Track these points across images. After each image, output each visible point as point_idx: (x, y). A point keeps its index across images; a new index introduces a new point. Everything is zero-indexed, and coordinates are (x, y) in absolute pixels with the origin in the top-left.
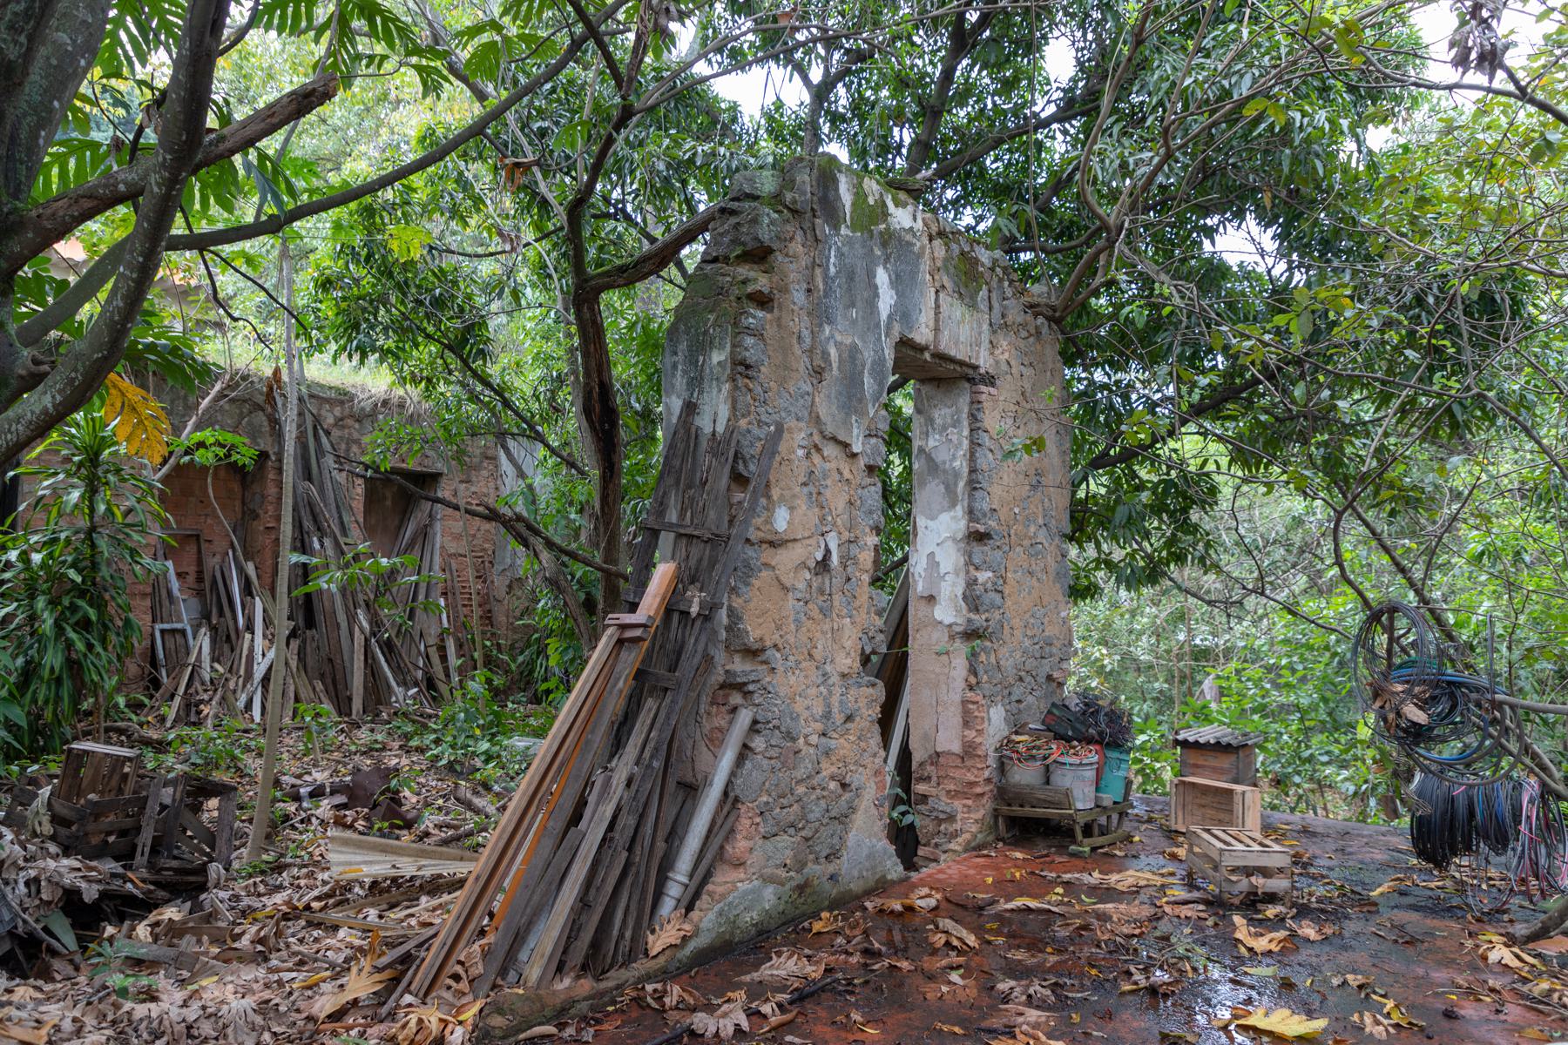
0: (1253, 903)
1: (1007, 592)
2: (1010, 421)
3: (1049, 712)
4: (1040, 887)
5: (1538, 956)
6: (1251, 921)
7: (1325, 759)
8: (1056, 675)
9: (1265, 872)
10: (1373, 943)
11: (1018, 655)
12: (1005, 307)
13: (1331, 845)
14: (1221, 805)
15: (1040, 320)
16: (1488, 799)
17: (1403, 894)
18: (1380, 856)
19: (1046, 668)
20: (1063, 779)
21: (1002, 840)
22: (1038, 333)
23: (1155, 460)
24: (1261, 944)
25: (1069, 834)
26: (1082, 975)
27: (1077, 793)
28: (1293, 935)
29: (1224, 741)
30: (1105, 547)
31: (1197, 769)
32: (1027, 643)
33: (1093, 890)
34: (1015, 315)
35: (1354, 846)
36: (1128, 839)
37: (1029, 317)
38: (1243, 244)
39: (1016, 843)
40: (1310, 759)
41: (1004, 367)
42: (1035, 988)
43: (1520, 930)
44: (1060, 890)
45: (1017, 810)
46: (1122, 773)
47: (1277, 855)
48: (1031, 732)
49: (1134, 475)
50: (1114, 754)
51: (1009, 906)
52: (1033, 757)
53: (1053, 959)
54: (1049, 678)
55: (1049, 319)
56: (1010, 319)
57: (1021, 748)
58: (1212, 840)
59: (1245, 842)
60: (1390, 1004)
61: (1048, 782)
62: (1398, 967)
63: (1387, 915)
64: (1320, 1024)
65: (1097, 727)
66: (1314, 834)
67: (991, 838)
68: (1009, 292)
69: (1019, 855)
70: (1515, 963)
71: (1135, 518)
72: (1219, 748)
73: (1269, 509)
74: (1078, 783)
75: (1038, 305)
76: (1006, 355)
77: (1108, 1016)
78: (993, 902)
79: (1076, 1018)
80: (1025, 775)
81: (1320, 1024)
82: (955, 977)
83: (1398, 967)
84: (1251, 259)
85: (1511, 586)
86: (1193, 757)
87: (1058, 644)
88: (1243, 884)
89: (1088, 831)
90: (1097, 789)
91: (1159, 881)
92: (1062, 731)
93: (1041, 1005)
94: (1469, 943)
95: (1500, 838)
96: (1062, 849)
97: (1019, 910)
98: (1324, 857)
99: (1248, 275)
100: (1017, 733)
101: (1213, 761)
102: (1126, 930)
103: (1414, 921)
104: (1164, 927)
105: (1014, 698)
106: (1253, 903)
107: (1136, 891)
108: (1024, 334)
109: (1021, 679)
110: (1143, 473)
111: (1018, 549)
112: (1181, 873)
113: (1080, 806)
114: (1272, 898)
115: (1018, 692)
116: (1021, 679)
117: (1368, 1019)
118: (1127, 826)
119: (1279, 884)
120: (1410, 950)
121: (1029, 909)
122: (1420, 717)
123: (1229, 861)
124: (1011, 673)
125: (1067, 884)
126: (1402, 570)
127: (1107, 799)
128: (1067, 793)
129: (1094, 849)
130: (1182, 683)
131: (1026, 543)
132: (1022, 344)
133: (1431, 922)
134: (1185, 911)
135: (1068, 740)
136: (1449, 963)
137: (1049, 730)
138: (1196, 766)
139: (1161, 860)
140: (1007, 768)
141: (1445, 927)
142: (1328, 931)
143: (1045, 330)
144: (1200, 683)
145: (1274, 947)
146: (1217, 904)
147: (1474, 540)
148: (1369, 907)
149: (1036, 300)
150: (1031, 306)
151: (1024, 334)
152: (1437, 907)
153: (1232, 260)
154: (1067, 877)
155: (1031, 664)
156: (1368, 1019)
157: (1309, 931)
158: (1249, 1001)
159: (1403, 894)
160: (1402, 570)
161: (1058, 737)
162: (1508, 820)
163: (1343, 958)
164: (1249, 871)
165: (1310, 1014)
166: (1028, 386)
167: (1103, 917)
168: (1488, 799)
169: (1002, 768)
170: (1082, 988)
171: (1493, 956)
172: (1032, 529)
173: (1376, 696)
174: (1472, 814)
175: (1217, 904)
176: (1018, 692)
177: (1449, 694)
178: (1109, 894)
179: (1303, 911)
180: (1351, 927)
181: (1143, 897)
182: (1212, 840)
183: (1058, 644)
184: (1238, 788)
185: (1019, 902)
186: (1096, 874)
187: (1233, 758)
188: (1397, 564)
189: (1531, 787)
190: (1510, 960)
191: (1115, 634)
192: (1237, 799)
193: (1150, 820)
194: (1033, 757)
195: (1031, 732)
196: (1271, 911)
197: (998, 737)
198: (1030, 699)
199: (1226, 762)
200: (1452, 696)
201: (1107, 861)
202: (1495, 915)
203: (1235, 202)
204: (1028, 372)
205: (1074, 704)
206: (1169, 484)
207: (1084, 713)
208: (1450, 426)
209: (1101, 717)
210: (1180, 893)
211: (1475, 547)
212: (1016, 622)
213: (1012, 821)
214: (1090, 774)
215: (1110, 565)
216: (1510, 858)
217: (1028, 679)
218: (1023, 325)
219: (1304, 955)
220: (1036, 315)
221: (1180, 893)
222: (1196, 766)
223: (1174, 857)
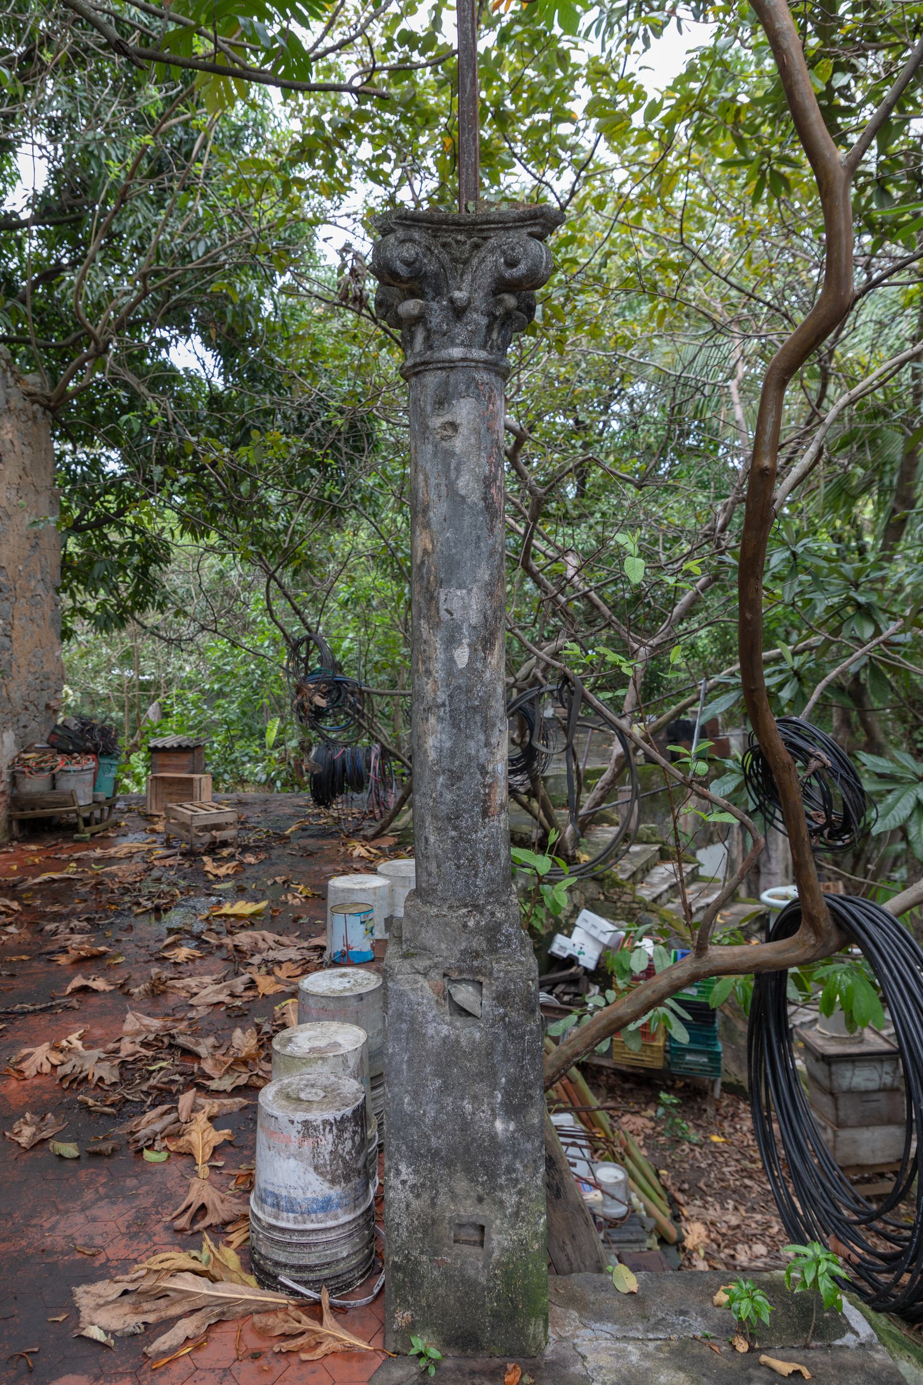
0: (213, 848)
1: (14, 636)
2: (14, 492)
3: (53, 733)
4: (61, 865)
5: (379, 848)
6: (214, 860)
7: (245, 759)
8: (52, 703)
9: (218, 827)
10: (288, 860)
11: (24, 688)
12: (8, 395)
13: (258, 809)
14: (185, 789)
15: (36, 406)
16: (353, 759)
17: (304, 830)
18: (289, 811)
19: (44, 700)
20: (66, 784)
21: (16, 839)
22: (35, 417)
23: (120, 527)
24: (222, 871)
25: (74, 828)
26: (105, 910)
27: (79, 793)
28: (241, 863)
29: (184, 744)
30: (78, 597)
31: (164, 767)
32: (31, 678)
33: (98, 861)
34: (17, 402)
35: (272, 807)
36: (117, 825)
37: (27, 404)
38: (189, 355)
39: (28, 840)
40: (234, 761)
41: (9, 446)
42: (75, 923)
43: (370, 832)
44: (73, 864)
45: (29, 814)
46: (112, 775)
47: (229, 815)
48: (37, 750)
49: (105, 536)
50: (106, 761)
51: (37, 880)
52: (42, 769)
53: (81, 906)
54: (48, 707)
55: (46, 408)
56: (12, 404)
57: (31, 763)
58: (185, 811)
59: (206, 807)
60: (301, 887)
61: (54, 788)
62: (304, 868)
63: (295, 844)
64: (263, 904)
65: (91, 740)
66: (246, 804)
67: (6, 839)
68: (11, 381)
69: (33, 847)
70: (366, 854)
71: (112, 573)
72: (181, 750)
73: (196, 563)
74: (80, 783)
75: (35, 394)
76: (10, 436)
77: (130, 928)
78: (23, 881)
79: (109, 934)
80: (35, 785)
81: (263, 904)
82: (11, 929)
83: (304, 868)
84: (194, 365)
85: (367, 624)
86: (160, 759)
87: (53, 678)
88: (207, 837)
89: (87, 822)
90: (94, 789)
91: (146, 847)
92: (64, 747)
93: (82, 931)
94: (342, 849)
95: (359, 783)
96: (67, 839)
97: (46, 882)
98: (254, 815)
99: (192, 379)
100: (25, 752)
101: (175, 760)
102: (130, 880)
103: (311, 843)
104: (156, 873)
105: (21, 724)
106: (213, 848)
107: (130, 857)
108: (24, 418)
109: (26, 708)
110: (114, 536)
111: (22, 600)
112: (160, 839)
113: (82, 803)
114: (225, 844)
115: (24, 719)
116: (26, 708)
117: (290, 897)
118: (114, 817)
119: (229, 834)
120: (310, 859)
121: (53, 881)
122: (321, 702)
123: (198, 823)
124: (19, 703)
125: (78, 860)
126: (298, 612)
127: (102, 796)
128: (72, 794)
129: (93, 835)
130: (130, 711)
131: (28, 595)
132: (22, 426)
133: (321, 842)
134: (168, 862)
135: (70, 753)
136: (332, 861)
137: (53, 747)
138: (164, 766)
139: (144, 835)
140: (19, 780)
141: (327, 844)
142: (262, 857)
143: (39, 415)
144: (145, 710)
145: (230, 872)
146: (190, 854)
147: (343, 591)
148: (284, 839)
149: (30, 388)
150: (29, 394)
151: (24, 418)
152: (324, 834)
153: (179, 366)
154: (76, 855)
155: (34, 695)
156: (290, 897)
157: (250, 859)
158: (219, 902)
159: (304, 830)
160: (298, 612)
161: (61, 751)
162: (365, 770)
163: (272, 870)
164: (206, 828)
165: (257, 901)
166: (27, 462)
167: (112, 876)
168: (353, 759)
169: (14, 781)
170: (108, 917)
171: (355, 853)
172: (33, 583)
173: (298, 692)
174: (344, 770)
175: (190, 854)
176: (24, 719)
177: (337, 688)
178: (110, 861)
179: (245, 849)
180: (275, 853)
181: (137, 858)
182: (185, 811)
183: (53, 678)
184: (196, 776)
185: (45, 877)
186: (98, 850)
187: (190, 756)
188: (295, 608)
189: (376, 749)
190: (364, 853)
191: (92, 668)
192: (196, 784)
193: (130, 811)
194: (42, 769)
195: (37, 750)
196: (225, 852)
197: (10, 757)
198: (34, 724)
199: (185, 760)
200: (339, 690)
201: (104, 841)
202: (354, 834)
203: (177, 317)
204: (27, 450)
205: (73, 724)
206: (134, 545)
207: (82, 731)
208: (329, 512)
209: (96, 733)
210: (161, 852)
211: (343, 596)
212: (22, 661)
213: (22, 823)
214: (89, 777)
215: (83, 612)
216: (365, 795)
217: (32, 708)
218: (23, 410)
219: (249, 872)
220: (33, 402)
221: (161, 852)
222: (164, 766)
223: (153, 831)
